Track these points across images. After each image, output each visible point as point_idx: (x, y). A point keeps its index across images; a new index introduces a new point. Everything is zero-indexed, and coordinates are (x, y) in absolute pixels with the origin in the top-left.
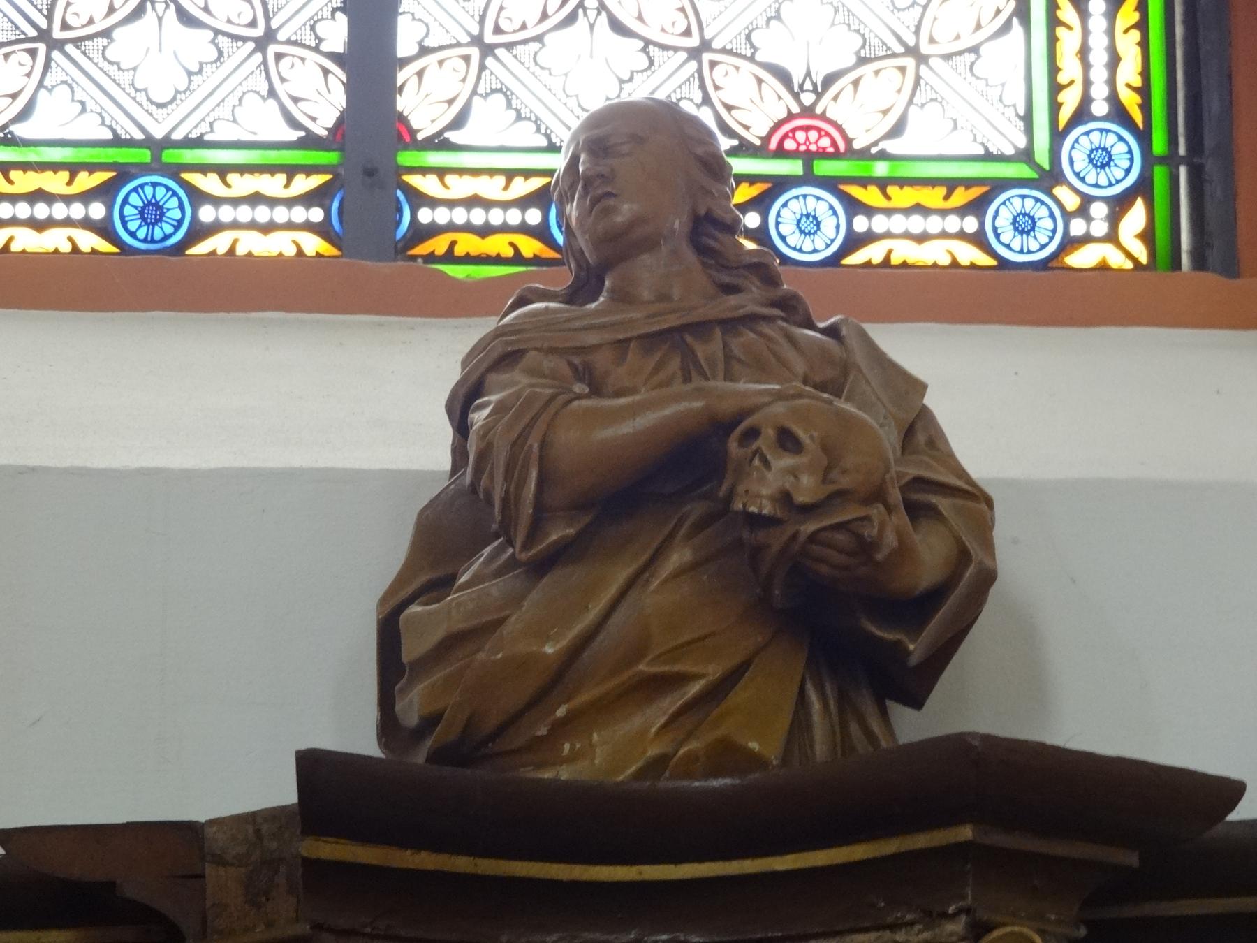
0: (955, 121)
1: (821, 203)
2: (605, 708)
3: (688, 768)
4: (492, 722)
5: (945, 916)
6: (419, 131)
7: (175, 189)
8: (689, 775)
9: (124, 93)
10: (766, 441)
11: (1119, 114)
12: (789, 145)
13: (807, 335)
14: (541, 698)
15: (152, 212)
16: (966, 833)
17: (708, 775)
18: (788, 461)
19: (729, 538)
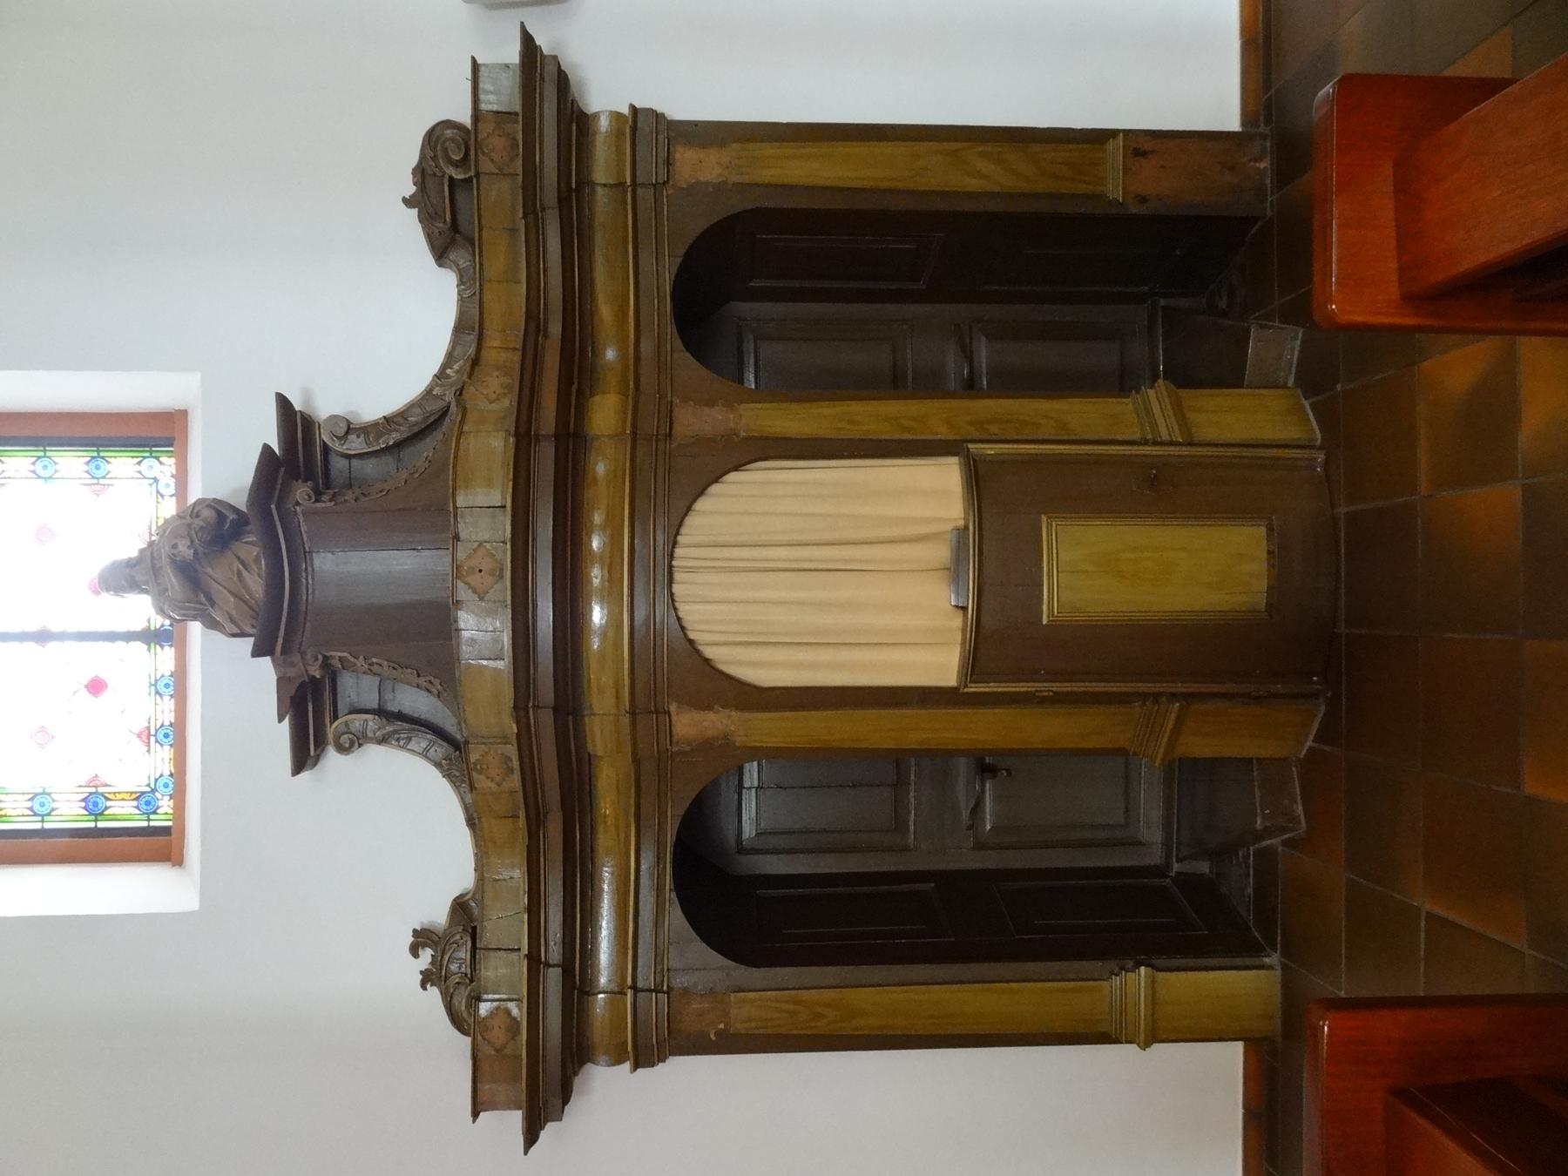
2: (246, 587)
3: (260, 569)
4: (252, 613)
5: (295, 511)
8: (261, 569)
10: (175, 552)
11: (139, 463)
14: (245, 602)
15: (167, 686)
16: (273, 507)
17: (261, 564)
18: (180, 547)
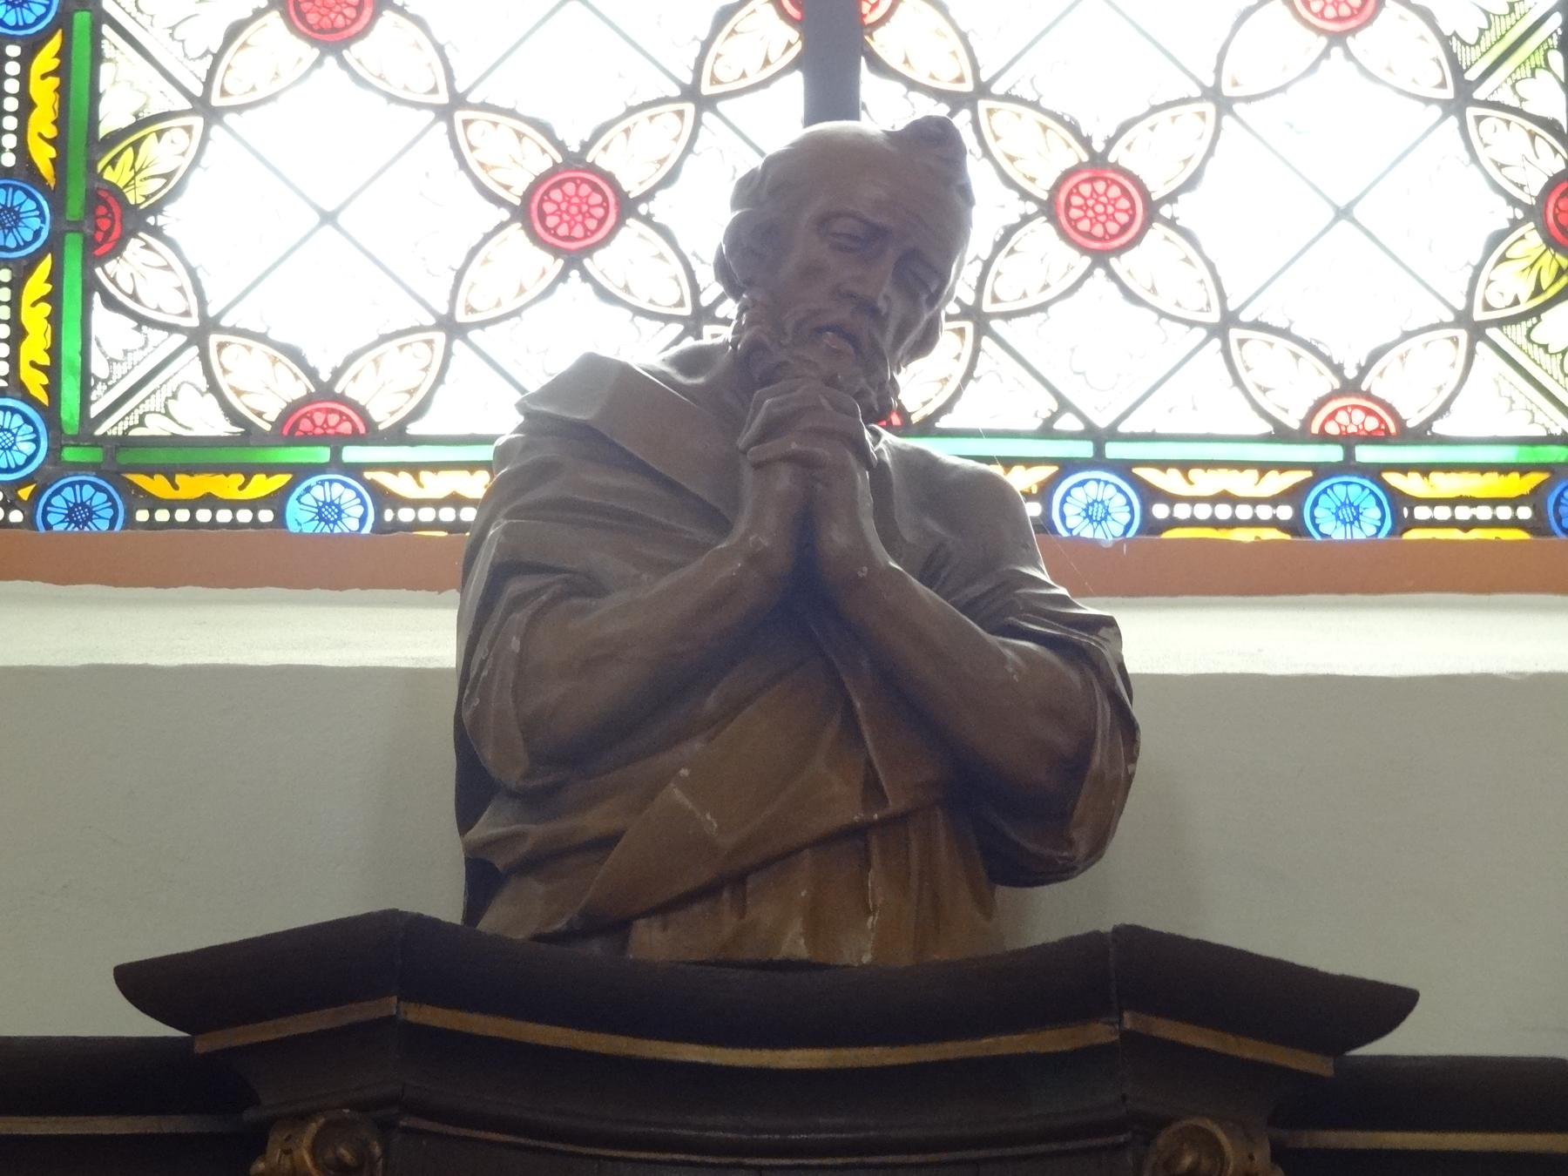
0: (1510, 398)
1: (1355, 490)
6: (380, 423)
7: (1327, 485)
9: (122, 381)
12: (1332, 429)
13: (1021, 646)
19: (803, 894)
